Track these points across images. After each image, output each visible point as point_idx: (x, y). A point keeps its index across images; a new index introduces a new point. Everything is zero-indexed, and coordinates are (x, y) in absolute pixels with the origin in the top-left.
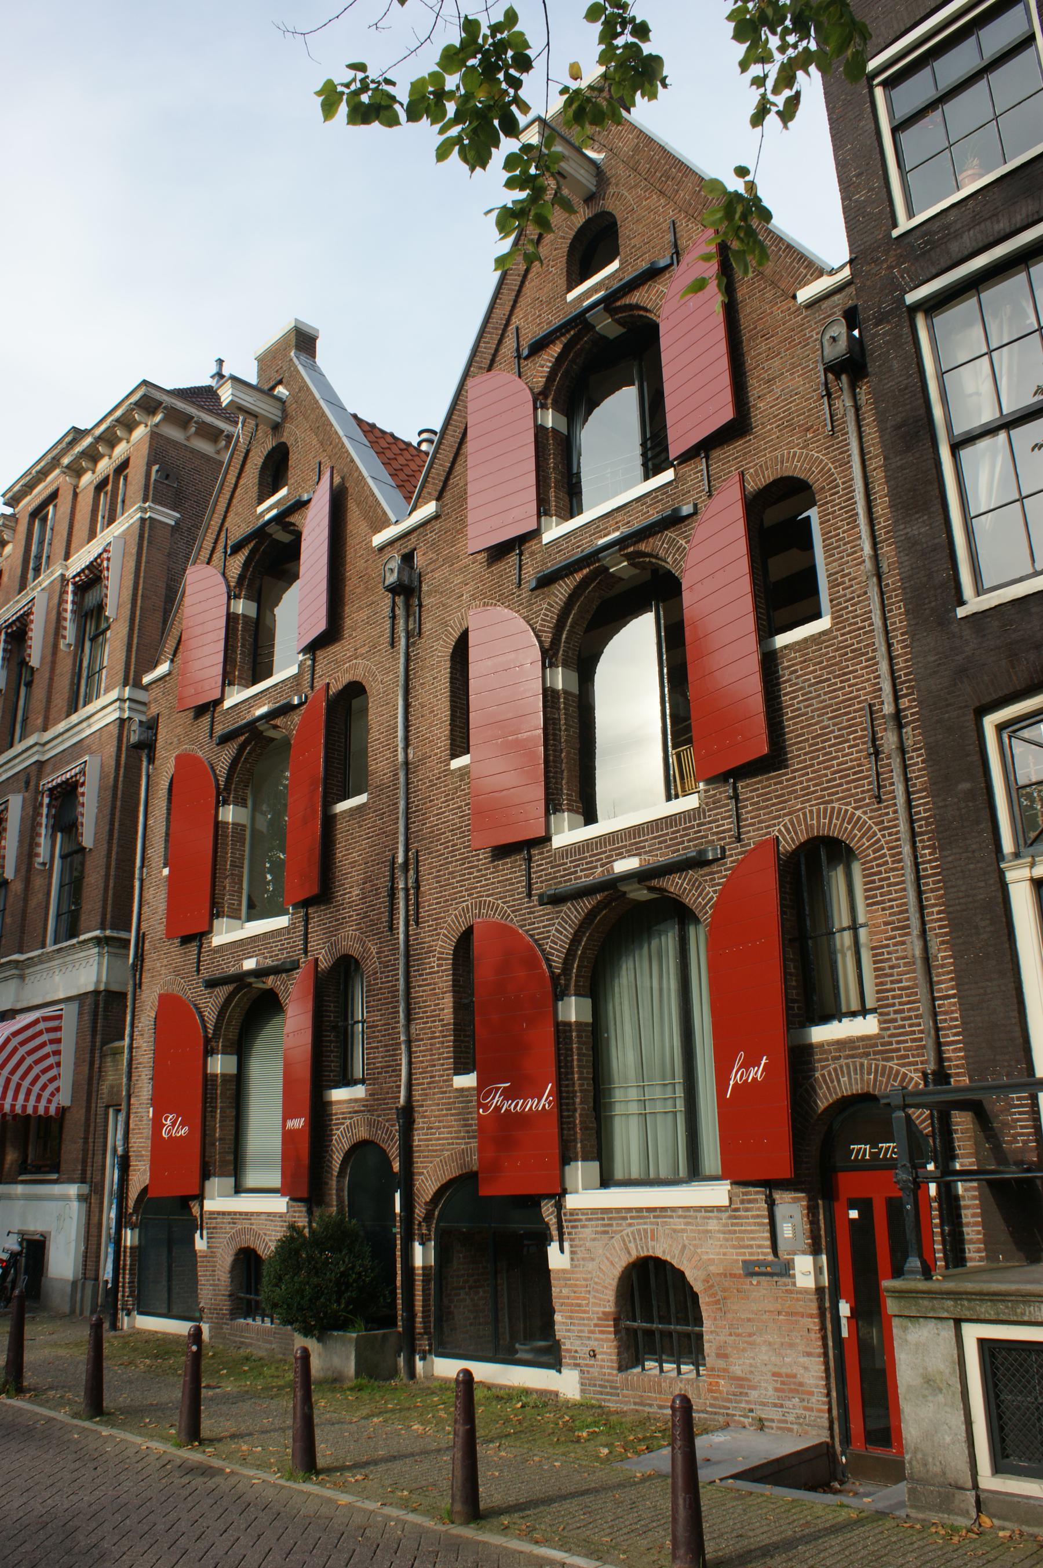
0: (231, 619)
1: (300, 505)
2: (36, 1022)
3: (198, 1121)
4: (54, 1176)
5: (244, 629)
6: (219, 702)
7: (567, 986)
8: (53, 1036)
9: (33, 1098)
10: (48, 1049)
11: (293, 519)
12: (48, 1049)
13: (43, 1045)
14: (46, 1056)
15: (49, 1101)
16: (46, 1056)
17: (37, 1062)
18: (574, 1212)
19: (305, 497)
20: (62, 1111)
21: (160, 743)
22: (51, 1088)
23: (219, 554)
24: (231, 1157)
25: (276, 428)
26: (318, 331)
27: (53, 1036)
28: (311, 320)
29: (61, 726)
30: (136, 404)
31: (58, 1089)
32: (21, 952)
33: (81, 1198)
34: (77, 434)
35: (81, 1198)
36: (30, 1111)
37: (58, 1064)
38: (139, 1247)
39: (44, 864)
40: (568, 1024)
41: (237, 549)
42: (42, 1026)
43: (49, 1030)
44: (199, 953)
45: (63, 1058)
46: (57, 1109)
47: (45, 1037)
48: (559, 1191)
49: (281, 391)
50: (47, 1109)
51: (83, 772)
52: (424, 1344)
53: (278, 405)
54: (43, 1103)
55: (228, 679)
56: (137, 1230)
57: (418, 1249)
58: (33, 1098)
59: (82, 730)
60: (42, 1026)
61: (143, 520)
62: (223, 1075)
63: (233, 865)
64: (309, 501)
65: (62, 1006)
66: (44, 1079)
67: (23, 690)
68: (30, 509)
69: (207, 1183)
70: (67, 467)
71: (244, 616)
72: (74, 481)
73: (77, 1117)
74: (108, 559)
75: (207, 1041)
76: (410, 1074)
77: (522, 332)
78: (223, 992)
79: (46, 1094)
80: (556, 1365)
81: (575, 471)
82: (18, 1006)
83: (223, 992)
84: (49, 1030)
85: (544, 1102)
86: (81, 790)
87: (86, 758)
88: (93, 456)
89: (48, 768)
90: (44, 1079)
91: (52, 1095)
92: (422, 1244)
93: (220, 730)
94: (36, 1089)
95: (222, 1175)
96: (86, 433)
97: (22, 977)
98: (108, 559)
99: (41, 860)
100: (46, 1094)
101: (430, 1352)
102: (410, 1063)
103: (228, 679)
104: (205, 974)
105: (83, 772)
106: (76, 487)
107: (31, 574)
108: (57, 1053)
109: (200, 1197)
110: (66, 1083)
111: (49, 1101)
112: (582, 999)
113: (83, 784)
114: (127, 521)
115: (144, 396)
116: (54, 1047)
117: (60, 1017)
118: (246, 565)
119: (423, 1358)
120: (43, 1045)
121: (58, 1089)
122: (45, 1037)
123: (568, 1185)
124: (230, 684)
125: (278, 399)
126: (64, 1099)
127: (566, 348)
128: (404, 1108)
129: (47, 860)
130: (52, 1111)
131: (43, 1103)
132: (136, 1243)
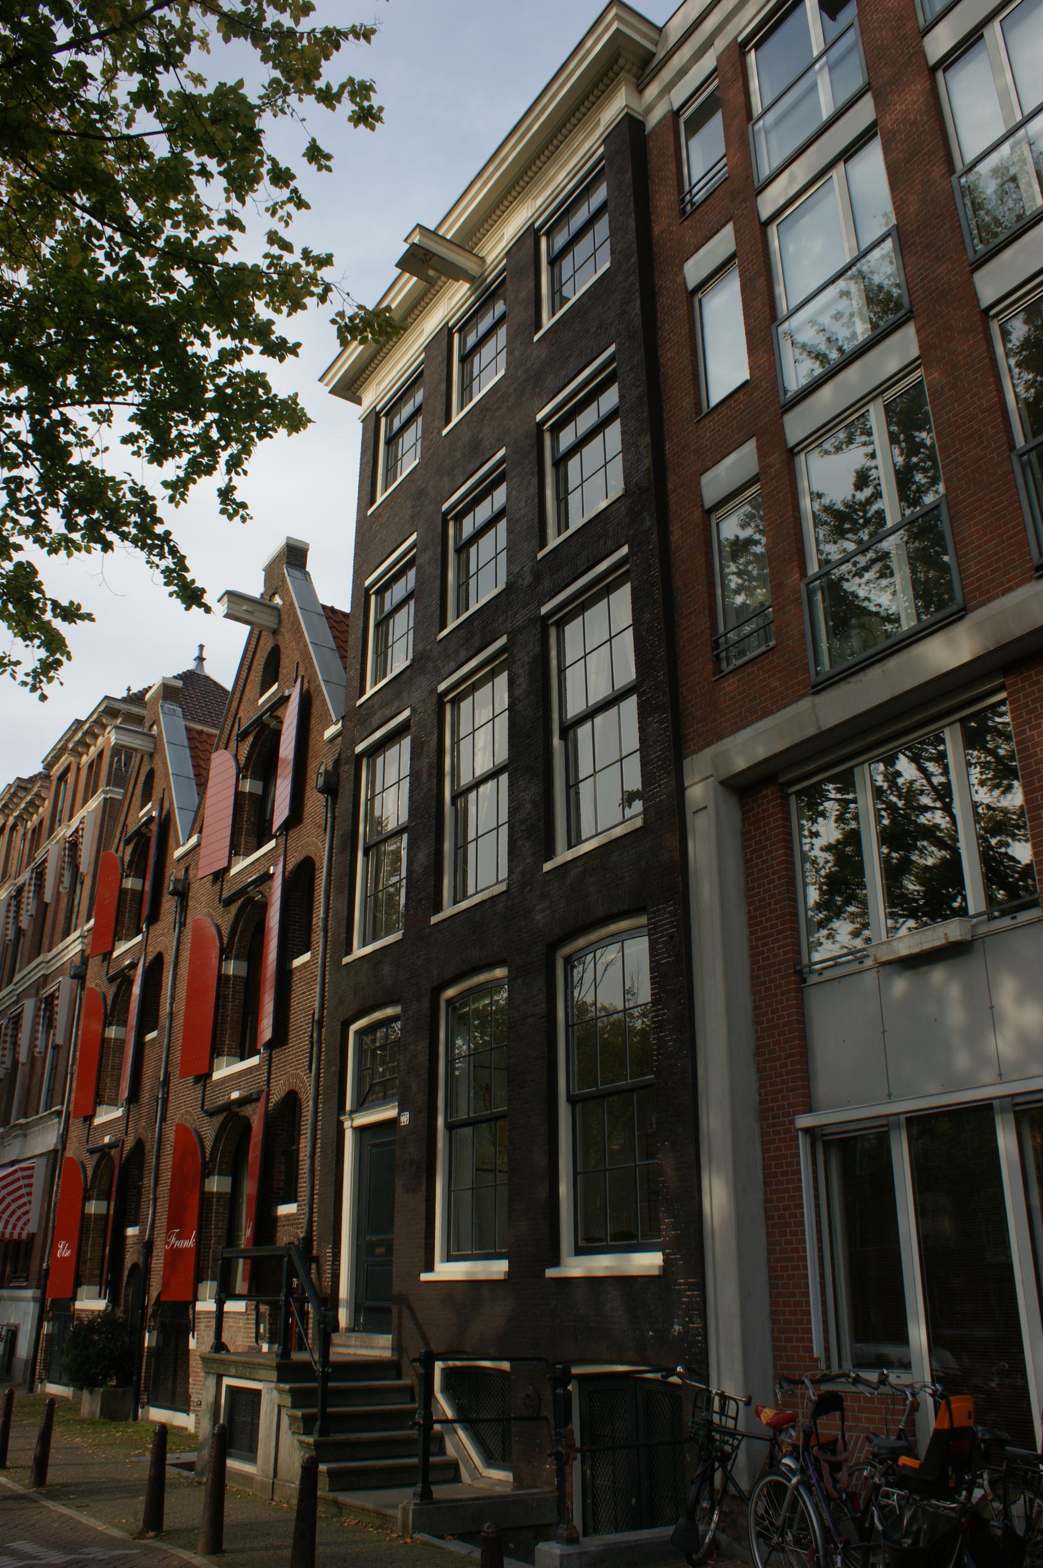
0: (239, 795)
1: (284, 700)
2: (16, 1171)
3: (76, 1246)
4: (24, 1284)
5: (132, 900)
6: (226, 870)
7: (213, 1169)
8: (27, 1181)
9: (10, 1227)
10: (23, 1191)
11: (278, 713)
12: (23, 1191)
13: (20, 1188)
14: (22, 1196)
15: (22, 1229)
16: (22, 1196)
17: (14, 1201)
18: (200, 1312)
19: (287, 693)
20: (32, 1236)
21: (88, 977)
22: (24, 1219)
23: (233, 744)
24: (98, 1272)
25: (275, 632)
26: (308, 545)
27: (27, 1181)
28: (300, 535)
29: (61, 946)
30: (103, 711)
31: (29, 1220)
32: (26, 1117)
33: (35, 1299)
34: (78, 723)
35: (35, 1299)
36: (16, 1236)
37: (30, 1202)
38: (158, 1347)
39: (40, 1053)
40: (212, 1193)
41: (243, 736)
42: (19, 1174)
43: (24, 1177)
44: (204, 1091)
45: (33, 1198)
46: (28, 1234)
47: (21, 1182)
48: (191, 1299)
49: (278, 600)
50: (20, 1234)
51: (58, 989)
52: (144, 1398)
53: (275, 613)
54: (18, 1230)
55: (236, 849)
56: (155, 1333)
57: (46, 1324)
58: (10, 1227)
59: (62, 958)
60: (19, 1174)
61: (105, 799)
62: (95, 1215)
63: (113, 1068)
64: (289, 696)
65: (34, 1160)
66: (19, 1212)
67: (79, 887)
68: (58, 774)
69: (79, 1290)
70: (72, 750)
71: (132, 890)
72: (77, 760)
73: (39, 1240)
74: (83, 829)
75: (86, 1191)
76: (153, 1220)
77: (242, 721)
78: (97, 1156)
79: (20, 1224)
80: (187, 1411)
81: (268, 817)
82: (21, 1158)
83: (97, 1156)
84: (24, 1177)
85: (189, 1243)
86: (56, 1002)
87: (60, 979)
88: (84, 744)
89: (50, 980)
90: (19, 1212)
91: (25, 1224)
92: (149, 1332)
93: (112, 972)
94: (13, 1220)
95: (90, 1284)
96: (84, 723)
97: (25, 1136)
98: (83, 829)
99: (38, 1050)
100: (20, 1224)
101: (148, 1403)
102: (154, 1213)
103: (236, 849)
104: (90, 1146)
105: (58, 989)
106: (79, 764)
107: (57, 823)
108: (29, 1194)
109: (74, 1299)
110: (34, 1216)
111: (22, 1229)
112: (223, 1178)
113: (57, 998)
114: (94, 803)
115: (106, 707)
116: (28, 1190)
117: (32, 1168)
118: (253, 746)
119: (143, 1407)
120: (20, 1188)
121: (29, 1220)
122: (21, 1182)
123: (200, 1296)
124: (236, 855)
125: (275, 608)
126: (32, 1228)
127: (136, 845)
128: (147, 1242)
129: (43, 1050)
130: (24, 1236)
131: (18, 1230)
132: (154, 1344)
